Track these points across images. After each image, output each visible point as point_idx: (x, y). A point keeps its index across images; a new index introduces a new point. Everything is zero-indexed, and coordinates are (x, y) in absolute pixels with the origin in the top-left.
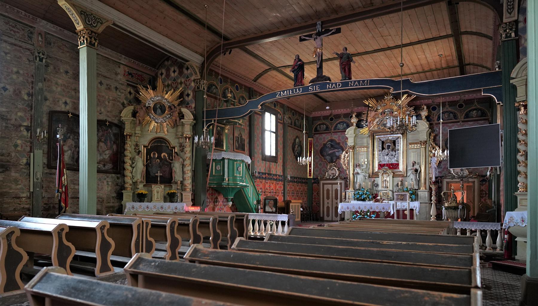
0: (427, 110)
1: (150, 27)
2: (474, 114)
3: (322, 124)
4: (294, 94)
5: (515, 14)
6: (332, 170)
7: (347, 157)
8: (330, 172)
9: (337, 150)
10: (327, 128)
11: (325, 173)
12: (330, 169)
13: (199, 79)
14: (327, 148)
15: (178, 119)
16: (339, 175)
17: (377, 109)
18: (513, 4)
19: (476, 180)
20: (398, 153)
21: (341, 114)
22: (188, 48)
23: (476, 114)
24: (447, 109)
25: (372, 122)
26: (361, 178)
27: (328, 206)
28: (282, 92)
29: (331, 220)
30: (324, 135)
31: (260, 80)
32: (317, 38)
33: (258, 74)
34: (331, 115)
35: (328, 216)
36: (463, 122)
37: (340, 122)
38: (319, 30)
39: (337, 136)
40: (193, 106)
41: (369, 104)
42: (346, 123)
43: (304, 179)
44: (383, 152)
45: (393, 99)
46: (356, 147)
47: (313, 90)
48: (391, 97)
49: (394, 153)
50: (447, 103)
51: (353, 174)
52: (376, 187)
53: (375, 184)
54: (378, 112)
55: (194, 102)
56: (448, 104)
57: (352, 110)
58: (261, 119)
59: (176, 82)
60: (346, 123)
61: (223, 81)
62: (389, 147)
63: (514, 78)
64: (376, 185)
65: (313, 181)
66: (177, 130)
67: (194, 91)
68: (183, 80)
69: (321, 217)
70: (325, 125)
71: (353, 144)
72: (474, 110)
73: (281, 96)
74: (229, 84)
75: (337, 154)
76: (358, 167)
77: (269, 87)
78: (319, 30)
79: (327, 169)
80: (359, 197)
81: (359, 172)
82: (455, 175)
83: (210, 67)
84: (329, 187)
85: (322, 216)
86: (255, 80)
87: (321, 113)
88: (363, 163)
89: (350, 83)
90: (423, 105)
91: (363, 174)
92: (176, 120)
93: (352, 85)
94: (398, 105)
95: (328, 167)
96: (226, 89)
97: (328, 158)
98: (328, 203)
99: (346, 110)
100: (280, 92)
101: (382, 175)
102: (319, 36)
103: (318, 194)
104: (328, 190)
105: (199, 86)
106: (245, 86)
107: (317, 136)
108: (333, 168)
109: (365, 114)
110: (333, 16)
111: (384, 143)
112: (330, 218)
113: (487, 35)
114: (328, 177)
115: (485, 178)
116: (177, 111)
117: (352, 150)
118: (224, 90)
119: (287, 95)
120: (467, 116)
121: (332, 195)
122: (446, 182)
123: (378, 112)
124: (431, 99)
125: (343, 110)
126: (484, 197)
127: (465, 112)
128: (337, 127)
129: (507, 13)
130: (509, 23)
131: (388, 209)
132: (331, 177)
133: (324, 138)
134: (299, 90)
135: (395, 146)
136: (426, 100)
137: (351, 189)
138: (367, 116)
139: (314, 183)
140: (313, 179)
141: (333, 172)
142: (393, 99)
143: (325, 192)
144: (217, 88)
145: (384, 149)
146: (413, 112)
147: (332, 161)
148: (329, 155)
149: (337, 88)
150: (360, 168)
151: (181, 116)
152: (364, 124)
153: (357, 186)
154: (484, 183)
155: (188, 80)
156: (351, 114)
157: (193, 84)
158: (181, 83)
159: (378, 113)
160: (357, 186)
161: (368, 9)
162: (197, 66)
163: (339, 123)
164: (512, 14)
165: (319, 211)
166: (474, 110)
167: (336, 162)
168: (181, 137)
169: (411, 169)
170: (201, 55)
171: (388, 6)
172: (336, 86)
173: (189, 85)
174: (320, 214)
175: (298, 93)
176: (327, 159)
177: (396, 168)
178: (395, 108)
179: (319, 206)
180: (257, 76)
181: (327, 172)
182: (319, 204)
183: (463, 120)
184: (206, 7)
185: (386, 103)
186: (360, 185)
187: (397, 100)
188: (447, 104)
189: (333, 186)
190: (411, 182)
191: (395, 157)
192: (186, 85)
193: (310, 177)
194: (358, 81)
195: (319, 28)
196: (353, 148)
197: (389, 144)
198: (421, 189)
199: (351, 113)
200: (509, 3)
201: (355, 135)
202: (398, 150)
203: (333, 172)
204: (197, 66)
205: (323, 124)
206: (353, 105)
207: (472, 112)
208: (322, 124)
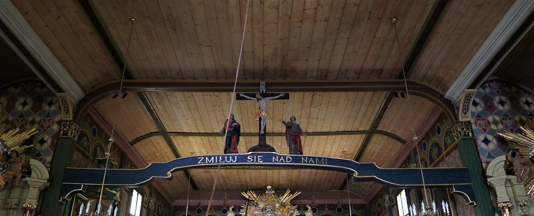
0: (312, 211)
1: (29, 22)
4: (226, 162)
5: (469, 115)
13: (70, 121)
15: (19, 175)
18: (468, 106)
22: (70, 73)
24: (327, 212)
28: (207, 158)
31: (137, 146)
32: (261, 100)
33: (139, 136)
34: (199, 205)
38: (263, 91)
40: (49, 159)
41: (249, 198)
45: (274, 194)
47: (253, 161)
48: (273, 192)
55: (52, 153)
56: (328, 207)
57: (225, 202)
58: (127, 198)
59: (24, 120)
61: (97, 134)
63: (491, 177)
66: (8, 196)
67: (56, 137)
68: (37, 119)
73: (205, 163)
74: (103, 139)
77: (144, 157)
78: (263, 91)
83: (89, 111)
86: (133, 143)
89: (303, 159)
90: (307, 205)
92: (15, 177)
93: (306, 161)
94: (281, 201)
96: (98, 146)
99: (218, 201)
100: (205, 157)
102: (264, 97)
105: (68, 131)
106: (119, 149)
109: (244, 208)
110: (280, 80)
113: (400, 137)
116: (20, 162)
118: (96, 147)
119: (215, 162)
124: (311, 199)
129: (463, 113)
130: (465, 122)
134: (233, 158)
142: (274, 194)
144: (88, 140)
146: (296, 212)
149: (286, 162)
151: (27, 171)
155: (47, 119)
156: (223, 207)
157: (55, 127)
158: (33, 123)
159: (258, 208)
161: (320, 81)
162: (71, 102)
164: (466, 115)
168: (15, 207)
170: (83, 88)
171: (341, 83)
172: (285, 161)
173: (47, 128)
175: (231, 162)
178: (277, 205)
180: (137, 138)
184: (133, 21)
185: (267, 197)
187: (279, 196)
192: (42, 126)
194: (313, 158)
195: (263, 89)
199: (224, 206)
200: (465, 104)
204: (71, 102)
206: (226, 196)
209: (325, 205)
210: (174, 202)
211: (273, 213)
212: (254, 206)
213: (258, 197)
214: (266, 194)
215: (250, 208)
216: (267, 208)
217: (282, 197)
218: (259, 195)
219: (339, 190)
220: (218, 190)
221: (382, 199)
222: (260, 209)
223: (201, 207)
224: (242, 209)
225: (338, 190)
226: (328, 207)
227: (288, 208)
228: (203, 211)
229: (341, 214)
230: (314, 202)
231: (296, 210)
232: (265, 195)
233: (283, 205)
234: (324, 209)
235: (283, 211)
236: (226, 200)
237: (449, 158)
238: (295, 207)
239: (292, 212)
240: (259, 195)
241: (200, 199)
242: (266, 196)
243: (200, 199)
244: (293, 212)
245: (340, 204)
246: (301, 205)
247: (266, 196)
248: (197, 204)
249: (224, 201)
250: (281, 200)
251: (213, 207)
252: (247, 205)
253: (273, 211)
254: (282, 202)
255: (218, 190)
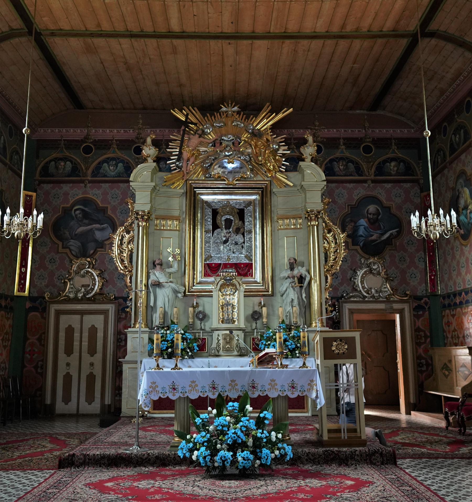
2: (392, 168)
3: (61, 159)
6: (83, 276)
7: (129, 243)
8: (79, 281)
9: (98, 226)
10: (75, 170)
11: (65, 283)
12: (77, 273)
14: (73, 219)
16: (101, 289)
17: (204, 133)
19: (406, 307)
20: (250, 238)
21: (112, 140)
23: (396, 169)
25: (192, 160)
26: (168, 296)
27: (68, 373)
29: (75, 412)
30: (66, 188)
34: (87, 138)
35: (67, 399)
36: (373, 181)
37: (108, 158)
39: (99, 192)
42: (122, 161)
43: (6, 297)
44: (215, 234)
45: (238, 113)
46: (153, 216)
49: (239, 238)
50: (342, 141)
51: (147, 286)
52: (201, 320)
53: (200, 312)
54: (204, 138)
60: (122, 161)
62: (228, 223)
64: (201, 316)
65: (28, 305)
69: (46, 405)
70: (71, 162)
71: (147, 208)
72: (392, 160)
75: (99, 235)
76: (158, 267)
79: (70, 274)
80: (167, 348)
81: (162, 279)
82: (367, 295)
84: (74, 320)
85: (48, 401)
87: (60, 131)
88: (170, 259)
91: (173, 285)
95: (75, 268)
97: (74, 244)
98: (68, 364)
99: (125, 132)
101: (220, 290)
103: (43, 340)
104: (70, 331)
107: (46, 187)
108: (88, 272)
109: (176, 140)
111: (218, 213)
112: (71, 407)
114: (72, 296)
115: (422, 301)
117: (144, 224)
120: (380, 171)
121: (81, 341)
122: (349, 310)
123: (204, 138)
125: (118, 132)
126: (423, 343)
127: (376, 163)
128: (101, 171)
131: (306, 387)
132: (80, 295)
133: (66, 194)
135: (244, 222)
136: (302, 131)
137: (140, 326)
138: (181, 147)
139: (33, 309)
140: (30, 298)
141: (86, 281)
142: (238, 113)
143: (62, 335)
145: (218, 227)
147: (84, 254)
148: (76, 237)
150: (162, 270)
152: (173, 163)
153: (157, 319)
154: (421, 313)
156: (136, 143)
160: (157, 319)
163: (107, 161)
165: (42, 389)
166: (392, 160)
167: (96, 256)
169: (289, 277)
174: (43, 396)
176: (72, 248)
177: (245, 275)
179: (43, 375)
181: (70, 280)
182: (44, 367)
183: (372, 177)
186: (165, 314)
187: (247, 118)
188: (341, 143)
189: (86, 318)
190: (289, 308)
191: (243, 247)
193: (21, 294)
196: (147, 217)
197: (228, 217)
198: (314, 325)
199: (137, 140)
201: (153, 184)
202: (250, 232)
203: (86, 281)
205: (65, 159)
206: (141, 121)
207: (388, 164)
208: (61, 159)
209: (339, 139)
210: (36, 132)
211: (237, 149)
212: (197, 136)
213: (206, 118)
214: (222, 114)
215: (189, 139)
216: (223, 140)
217: (254, 119)
218: (208, 115)
219: (367, 110)
220: (124, 109)
221: (444, 136)
222: (209, 141)
223: (91, 143)
224: (172, 143)
225: (365, 112)
226: (344, 144)
227: (267, 139)
228: (96, 149)
229: (366, 157)
230: (319, 134)
231: (284, 144)
232: (220, 115)
233: (256, 134)
234: (337, 148)
235: (256, 146)
236: (140, 129)
237: (466, 156)
238: (281, 138)
239: (275, 146)
240: (208, 115)
241: (88, 127)
242: (221, 117)
243: (88, 127)
244: (277, 147)
245: (370, 138)
246: (291, 138)
247: (221, 117)
248: (83, 137)
249: (137, 131)
250: (252, 124)
251: (115, 141)
252: (182, 132)
253: (236, 145)
254: (253, 129)
255: (124, 109)
